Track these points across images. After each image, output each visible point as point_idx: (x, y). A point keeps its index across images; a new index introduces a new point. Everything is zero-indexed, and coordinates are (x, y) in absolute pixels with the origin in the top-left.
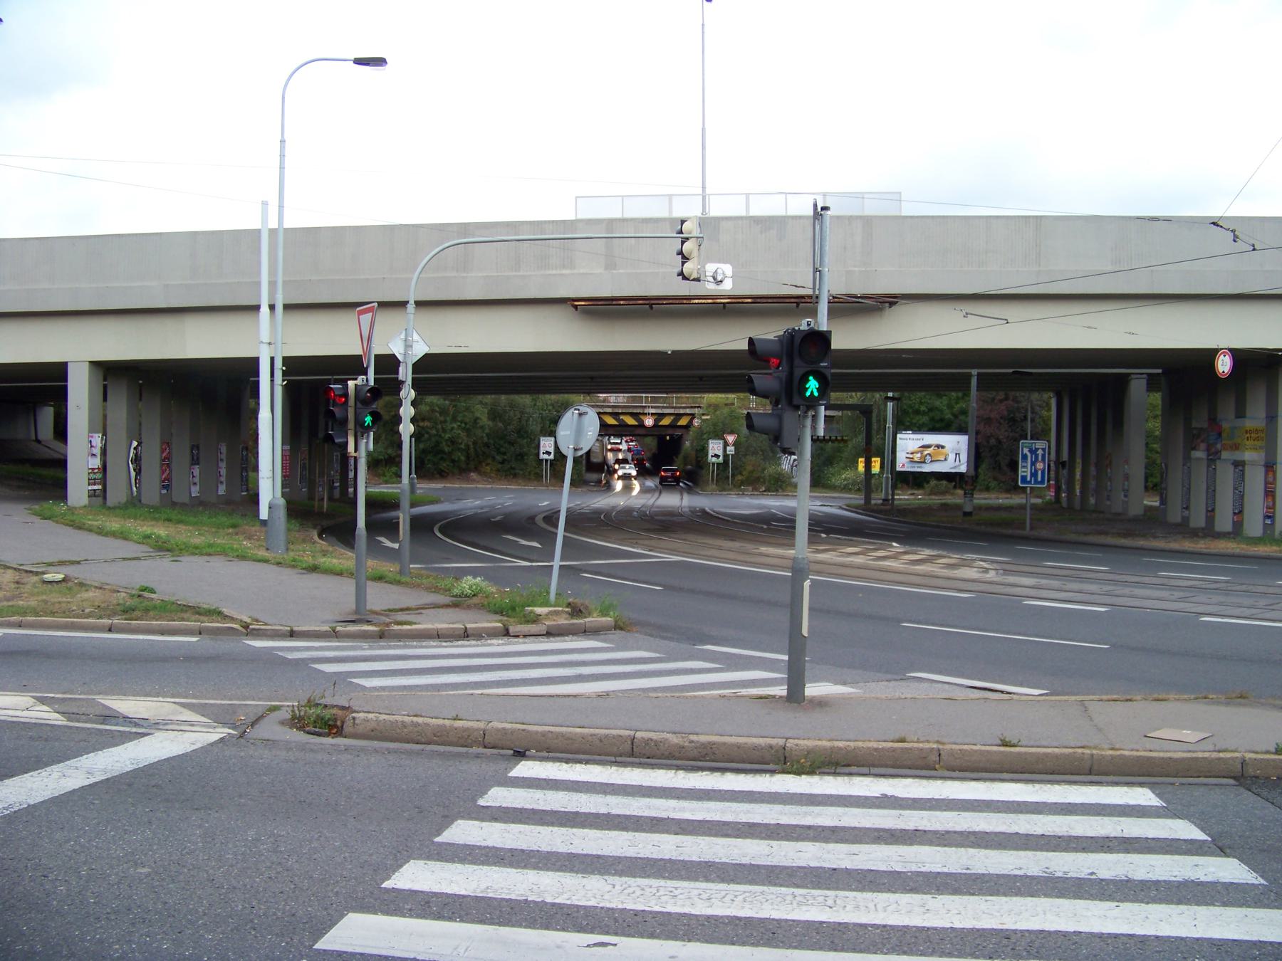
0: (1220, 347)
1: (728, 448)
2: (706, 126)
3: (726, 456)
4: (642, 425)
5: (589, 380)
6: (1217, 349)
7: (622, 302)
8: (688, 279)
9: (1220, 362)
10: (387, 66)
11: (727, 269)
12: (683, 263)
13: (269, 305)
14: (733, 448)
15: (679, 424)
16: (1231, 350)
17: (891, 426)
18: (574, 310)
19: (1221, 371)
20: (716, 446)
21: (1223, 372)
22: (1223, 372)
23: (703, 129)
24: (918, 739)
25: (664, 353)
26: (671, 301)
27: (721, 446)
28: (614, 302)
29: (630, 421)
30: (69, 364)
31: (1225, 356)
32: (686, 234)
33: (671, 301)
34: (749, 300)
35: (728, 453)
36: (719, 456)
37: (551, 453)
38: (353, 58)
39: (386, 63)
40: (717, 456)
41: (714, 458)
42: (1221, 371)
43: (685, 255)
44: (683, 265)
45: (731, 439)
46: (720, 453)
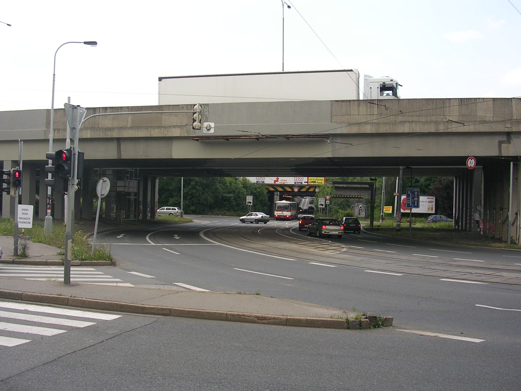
0: (469, 155)
1: (327, 201)
2: (284, 62)
3: (326, 205)
4: (293, 191)
5: (268, 171)
6: (467, 156)
7: (212, 138)
8: (195, 129)
9: (469, 162)
10: (97, 45)
11: (212, 125)
12: (193, 122)
13: (70, 139)
14: (329, 201)
15: (309, 191)
16: (474, 157)
17: (384, 192)
18: (197, 142)
19: (469, 166)
20: (321, 201)
21: (471, 166)
22: (471, 166)
23: (283, 63)
24: (283, 314)
25: (231, 159)
26: (232, 138)
27: (324, 200)
28: (210, 138)
29: (289, 189)
30: (4, 161)
31: (471, 160)
32: (195, 110)
33: (232, 138)
34: (265, 137)
35: (327, 203)
36: (323, 205)
37: (251, 202)
38: (84, 42)
39: (97, 44)
40: (322, 205)
41: (321, 206)
42: (469, 166)
43: (195, 119)
44: (193, 123)
45: (328, 197)
46: (324, 203)
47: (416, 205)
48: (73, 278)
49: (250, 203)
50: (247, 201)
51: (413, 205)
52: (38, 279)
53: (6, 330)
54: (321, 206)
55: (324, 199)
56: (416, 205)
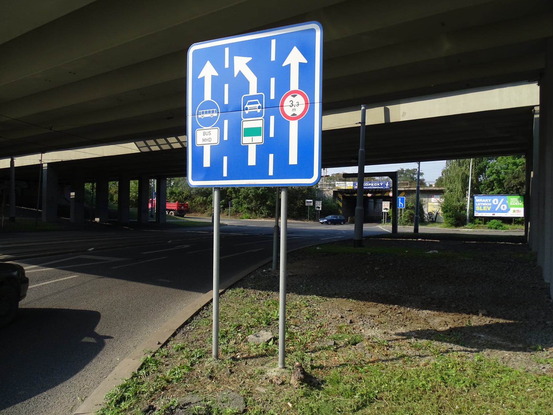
20: (386, 205)
47: (293, 159)
48: (27, 270)
49: (319, 208)
50: (383, 208)
51: (336, 296)
52: (182, 248)
53: (100, 277)
54: (385, 211)
55: (320, 202)
56: (293, 159)
